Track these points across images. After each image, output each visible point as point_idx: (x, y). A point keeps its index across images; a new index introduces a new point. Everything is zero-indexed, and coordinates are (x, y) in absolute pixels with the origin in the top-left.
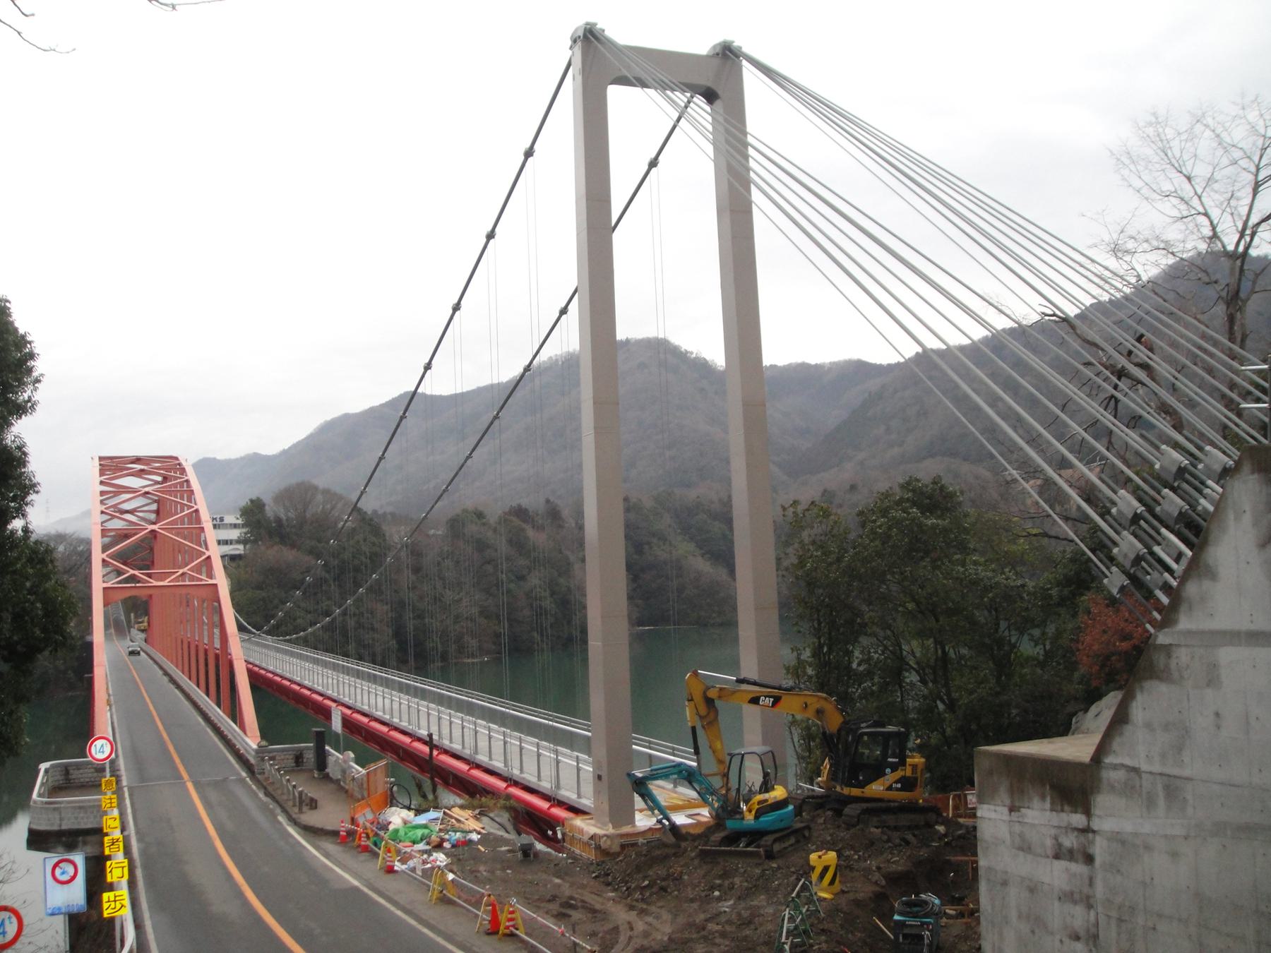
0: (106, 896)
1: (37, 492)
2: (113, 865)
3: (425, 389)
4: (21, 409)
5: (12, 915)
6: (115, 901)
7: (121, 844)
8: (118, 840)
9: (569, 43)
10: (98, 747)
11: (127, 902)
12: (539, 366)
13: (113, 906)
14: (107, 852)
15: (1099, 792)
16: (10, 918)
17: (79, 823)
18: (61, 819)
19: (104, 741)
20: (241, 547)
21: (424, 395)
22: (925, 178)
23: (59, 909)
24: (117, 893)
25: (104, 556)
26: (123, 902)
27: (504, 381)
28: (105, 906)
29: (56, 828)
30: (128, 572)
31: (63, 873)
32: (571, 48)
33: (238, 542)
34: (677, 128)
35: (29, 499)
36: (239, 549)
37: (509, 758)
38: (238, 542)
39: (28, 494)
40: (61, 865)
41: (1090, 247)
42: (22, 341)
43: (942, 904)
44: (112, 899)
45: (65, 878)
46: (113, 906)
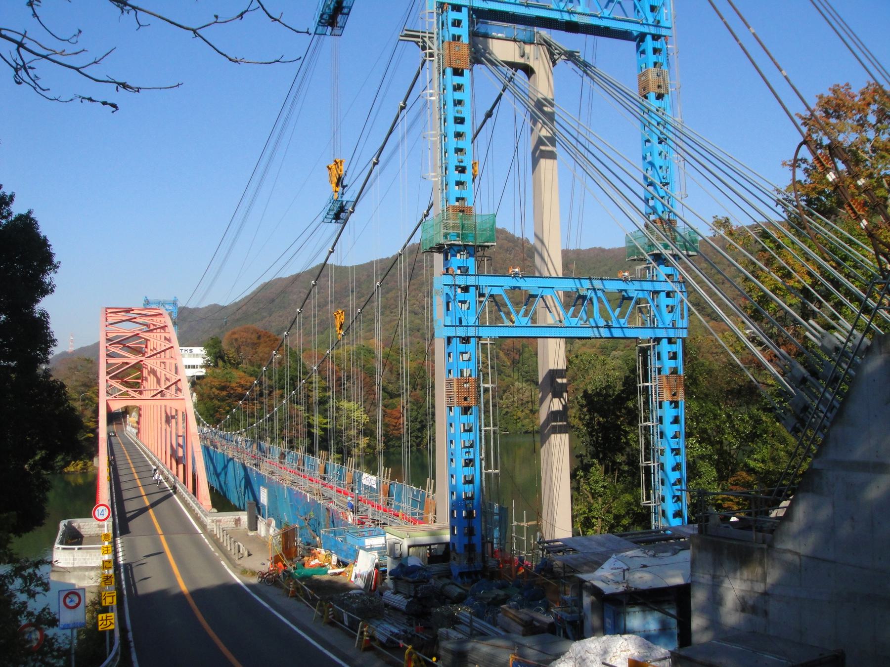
1: (56, 346)
3: (333, 261)
4: (46, 290)
7: (113, 580)
13: (105, 623)
17: (86, 563)
18: (74, 560)
19: (104, 508)
20: (204, 370)
21: (332, 266)
23: (68, 625)
24: (108, 615)
25: (108, 378)
27: (390, 257)
28: (100, 623)
29: (70, 566)
31: (71, 601)
33: (202, 367)
35: (50, 349)
36: (202, 372)
37: (566, 17)
39: (50, 347)
41: (797, 114)
42: (43, 243)
44: (104, 618)
45: (73, 604)
46: (105, 623)
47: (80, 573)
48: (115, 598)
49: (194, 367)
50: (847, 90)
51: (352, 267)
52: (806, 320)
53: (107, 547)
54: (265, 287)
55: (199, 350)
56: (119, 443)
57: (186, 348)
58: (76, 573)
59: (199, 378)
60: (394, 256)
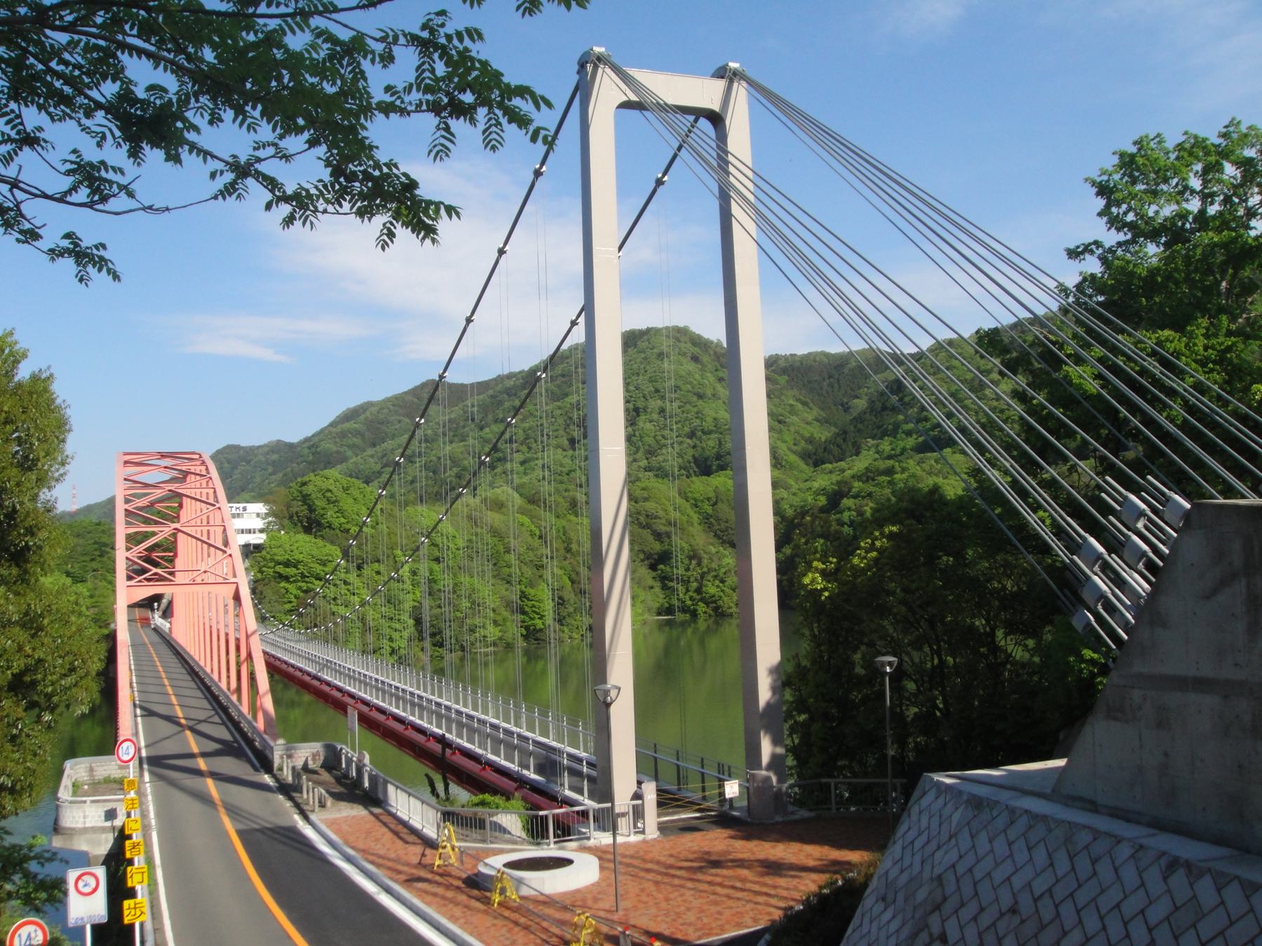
0: (126, 903)
2: (134, 871)
3: (451, 377)
5: (38, 929)
6: (135, 908)
7: (142, 848)
8: (138, 844)
9: (577, 68)
10: (125, 748)
11: (147, 909)
12: (570, 349)
13: (133, 913)
14: (128, 855)
15: (913, 490)
16: (36, 931)
19: (128, 743)
22: (219, 656)
26: (143, 910)
27: (526, 369)
28: (126, 913)
30: (151, 570)
31: (85, 885)
32: (578, 73)
33: (261, 531)
34: (678, 159)
36: (259, 539)
38: (261, 531)
40: (84, 878)
43: (795, 721)
44: (132, 906)
46: (133, 913)
47: (94, 836)
48: (146, 875)
49: (249, 531)
50: (1159, 142)
51: (472, 385)
52: (1144, 478)
53: (133, 800)
54: (350, 415)
55: (260, 508)
56: (145, 644)
57: (238, 505)
58: (88, 836)
59: (258, 547)
60: (531, 369)
